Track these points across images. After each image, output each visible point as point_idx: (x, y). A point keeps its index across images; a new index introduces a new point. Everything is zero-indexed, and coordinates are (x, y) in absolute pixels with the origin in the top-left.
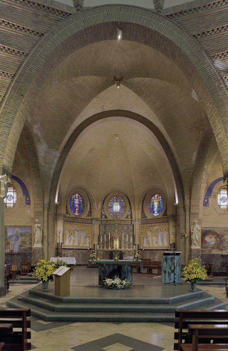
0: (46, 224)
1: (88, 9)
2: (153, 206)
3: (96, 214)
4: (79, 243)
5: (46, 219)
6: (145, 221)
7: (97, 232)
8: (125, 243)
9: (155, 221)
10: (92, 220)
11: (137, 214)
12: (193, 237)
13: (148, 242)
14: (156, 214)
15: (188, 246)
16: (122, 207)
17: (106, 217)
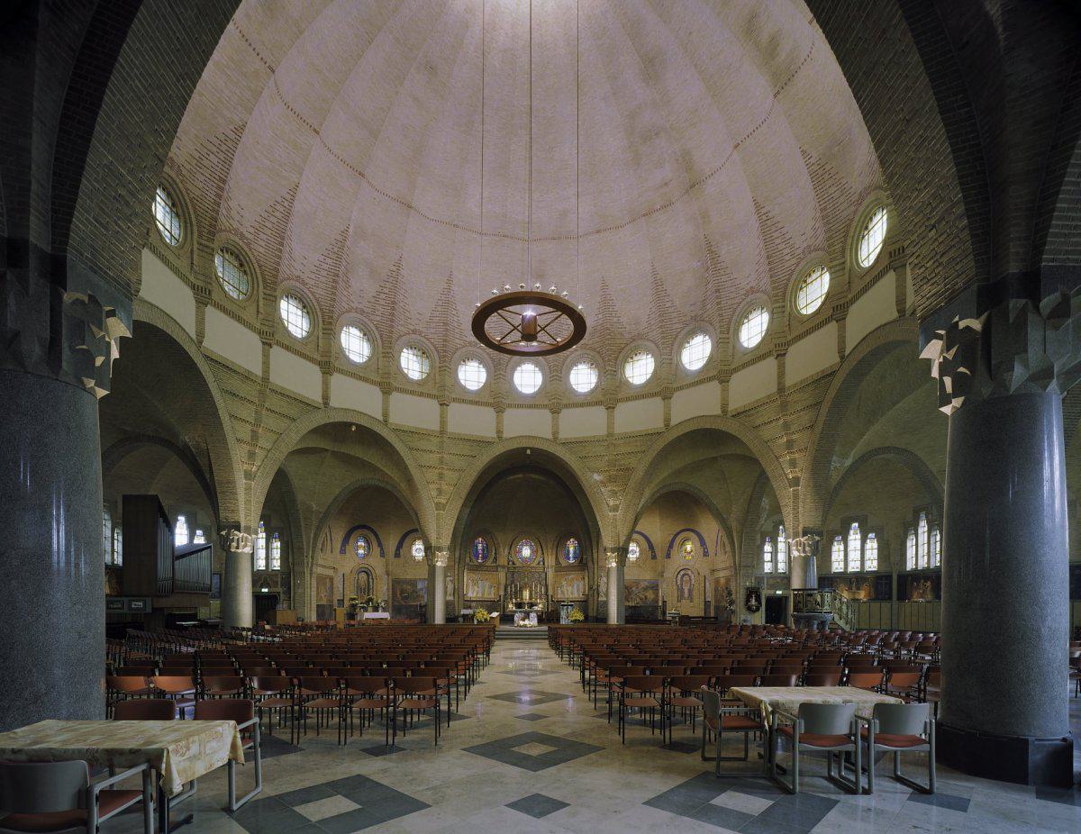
0: (456, 577)
1: (507, 439)
2: (569, 551)
3: (503, 561)
4: (483, 594)
5: (456, 572)
6: (559, 568)
7: (503, 581)
8: (536, 593)
9: (571, 568)
10: (497, 567)
11: (550, 560)
12: (600, 590)
13: (563, 592)
14: (572, 561)
15: (596, 598)
16: (533, 552)
17: (514, 563)
